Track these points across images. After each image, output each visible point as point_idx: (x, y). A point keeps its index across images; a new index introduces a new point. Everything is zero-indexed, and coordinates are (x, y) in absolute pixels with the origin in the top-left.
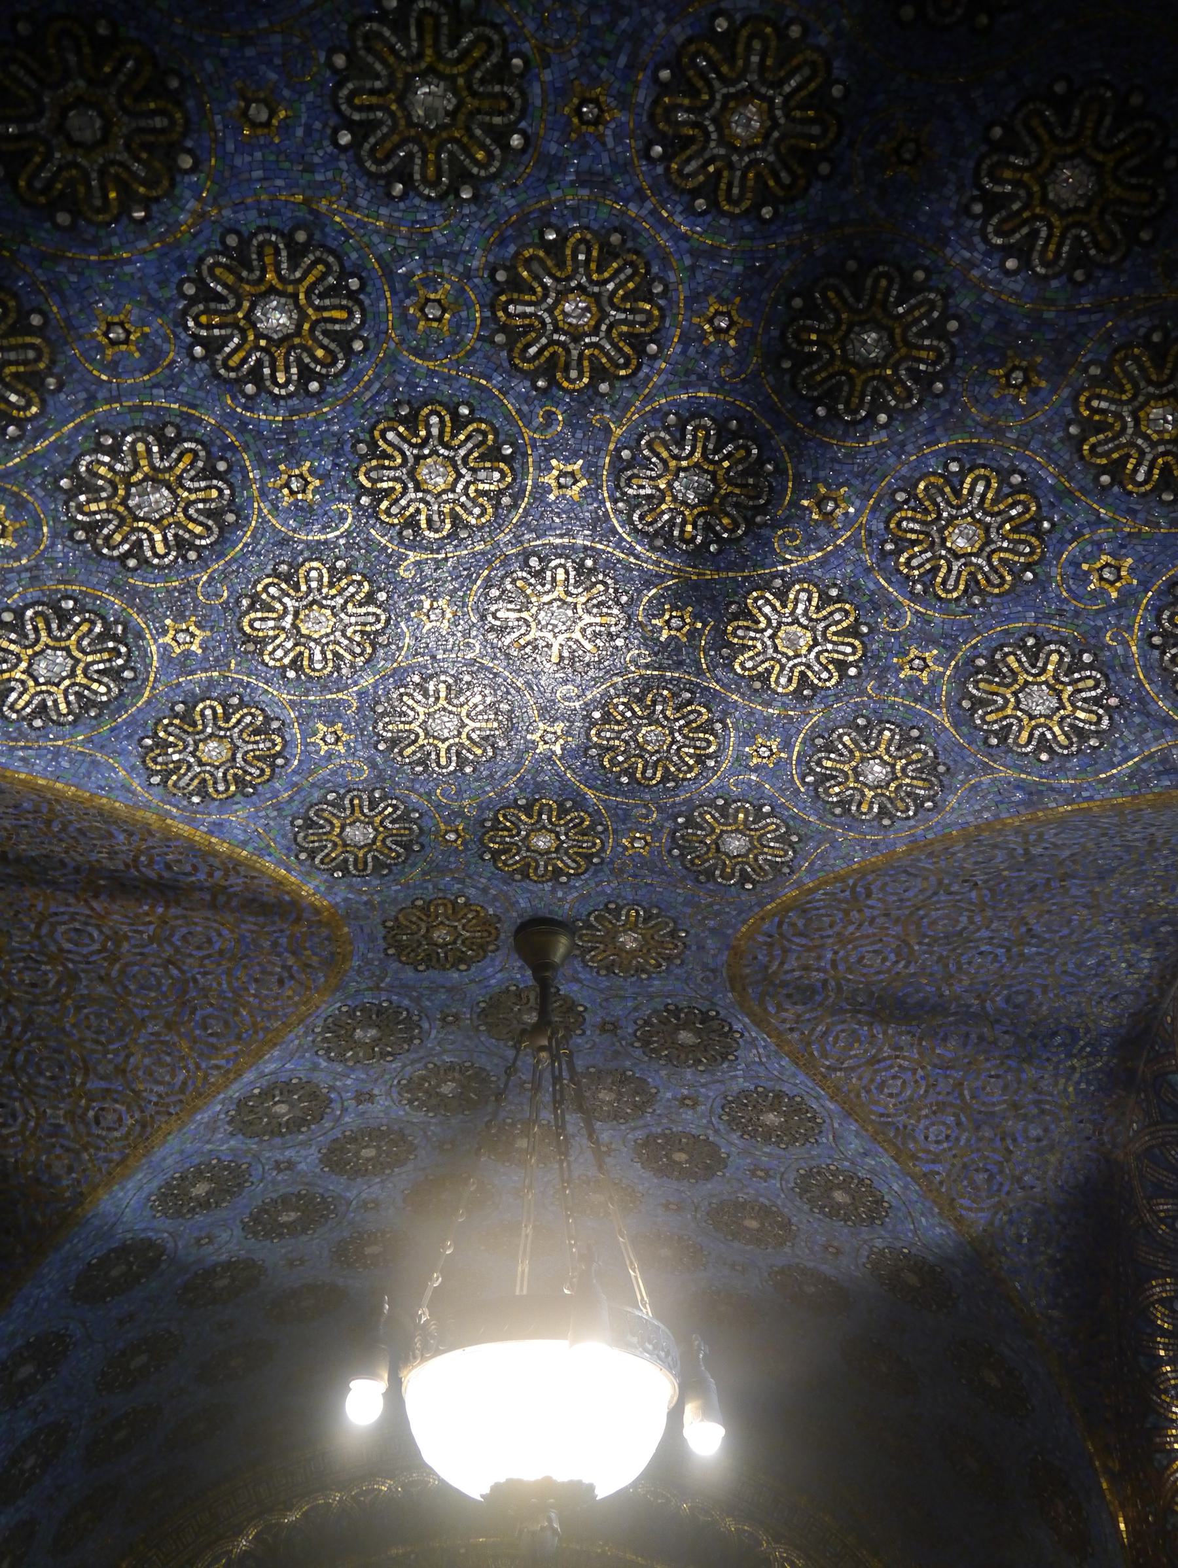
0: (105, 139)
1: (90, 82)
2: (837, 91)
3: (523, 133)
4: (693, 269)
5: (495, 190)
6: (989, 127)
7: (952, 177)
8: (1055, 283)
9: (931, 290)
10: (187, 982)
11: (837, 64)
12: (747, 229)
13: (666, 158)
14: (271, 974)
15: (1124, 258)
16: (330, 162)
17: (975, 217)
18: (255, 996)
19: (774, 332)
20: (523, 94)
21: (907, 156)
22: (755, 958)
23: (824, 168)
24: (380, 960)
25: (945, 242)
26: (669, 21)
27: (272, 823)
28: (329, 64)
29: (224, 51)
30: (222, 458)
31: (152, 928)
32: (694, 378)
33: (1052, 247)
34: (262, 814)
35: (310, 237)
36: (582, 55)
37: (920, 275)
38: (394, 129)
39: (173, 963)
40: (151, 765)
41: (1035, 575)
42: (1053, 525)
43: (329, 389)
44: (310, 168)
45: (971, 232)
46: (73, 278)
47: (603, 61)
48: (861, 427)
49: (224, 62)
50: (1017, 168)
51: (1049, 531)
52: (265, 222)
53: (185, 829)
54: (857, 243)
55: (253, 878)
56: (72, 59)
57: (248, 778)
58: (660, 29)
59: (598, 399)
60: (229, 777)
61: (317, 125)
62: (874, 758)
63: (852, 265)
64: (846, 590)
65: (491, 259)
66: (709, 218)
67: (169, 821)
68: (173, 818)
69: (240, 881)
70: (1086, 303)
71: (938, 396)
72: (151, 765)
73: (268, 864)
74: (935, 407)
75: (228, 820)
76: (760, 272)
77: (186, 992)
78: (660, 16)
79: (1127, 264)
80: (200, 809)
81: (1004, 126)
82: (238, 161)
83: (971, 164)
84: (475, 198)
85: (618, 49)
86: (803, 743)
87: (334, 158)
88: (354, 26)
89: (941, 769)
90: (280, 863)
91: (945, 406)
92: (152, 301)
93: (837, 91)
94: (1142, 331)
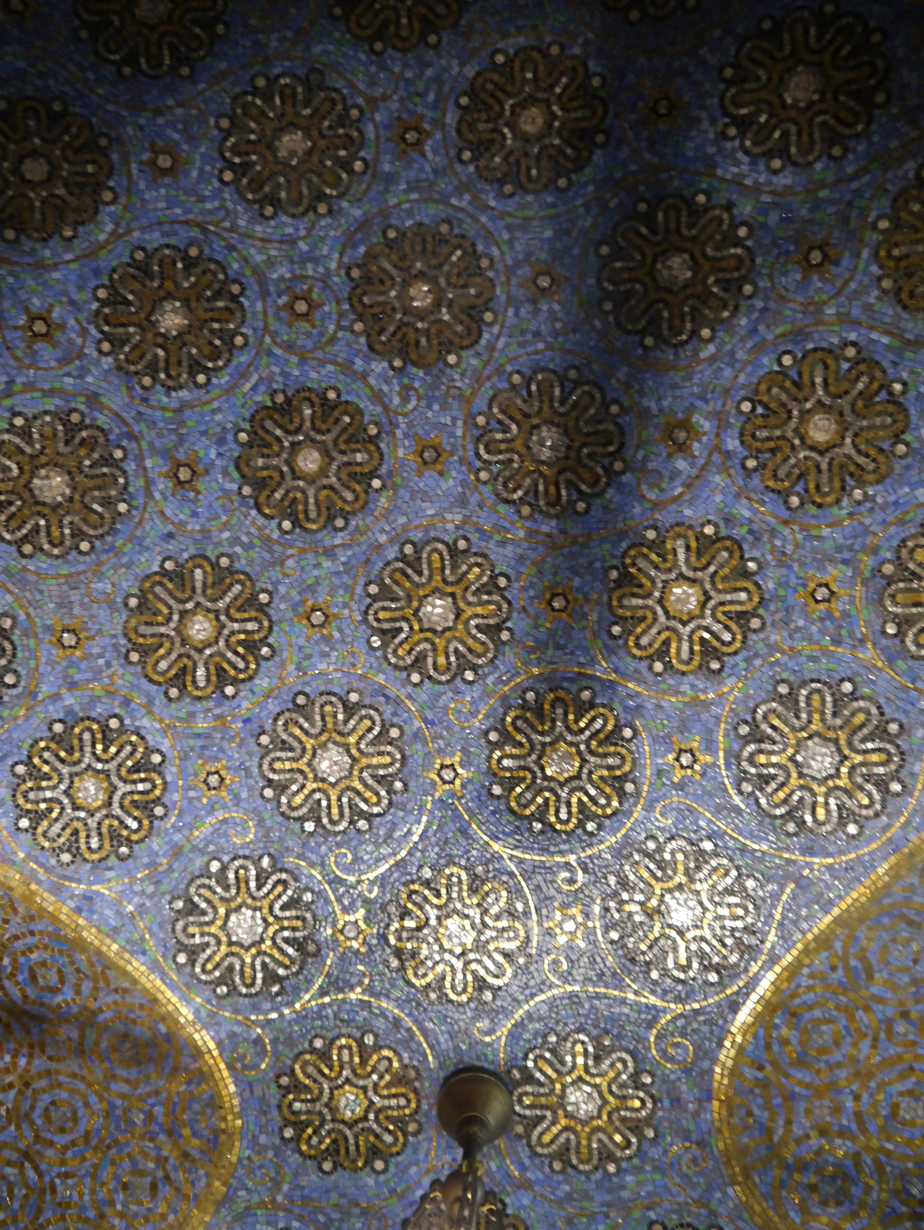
0: (49, 180)
1: (43, 140)
2: (596, 82)
3: (363, 159)
4: (511, 242)
5: (345, 204)
6: (721, 70)
7: (703, 115)
8: (818, 166)
9: (715, 207)
10: (43, 1191)
11: (591, 64)
12: (550, 199)
13: (474, 159)
14: (142, 1174)
15: (868, 124)
16: (217, 194)
17: (732, 139)
18: (122, 1215)
19: (591, 281)
20: (360, 132)
21: (663, 111)
22: (750, 1113)
23: (600, 138)
24: (275, 1148)
25: (713, 166)
26: (462, 64)
27: (148, 904)
28: (217, 126)
29: (142, 121)
30: (119, 447)
31: (12, 1094)
32: (529, 337)
33: (805, 138)
34: (137, 888)
35: (201, 251)
36: (401, 100)
37: (701, 198)
38: (418, 585)
39: (32, 1161)
40: (21, 801)
41: (907, 445)
42: (905, 384)
43: (214, 381)
44: (202, 199)
45: (733, 151)
46: (11, 280)
47: (417, 100)
48: (688, 347)
49: (141, 128)
50: (752, 91)
51: (903, 393)
52: (166, 241)
53: (49, 901)
54: (642, 188)
55: (125, 991)
56: (32, 123)
57: (125, 833)
58: (456, 70)
59: (448, 371)
60: (104, 830)
61: (208, 168)
62: (810, 737)
63: (643, 207)
64: (722, 524)
65: (346, 259)
66: (517, 198)
67: (33, 887)
68: (39, 883)
69: (110, 999)
70: (850, 170)
71: (749, 298)
72: (21, 801)
73: (137, 967)
74: (751, 308)
75: (97, 893)
76: (568, 232)
77: (40, 1211)
78: (454, 63)
79: (874, 127)
80: (69, 871)
81: (732, 66)
82: (147, 196)
83: (716, 101)
84: (330, 212)
85: (427, 90)
86: (726, 735)
87: (221, 191)
88: (235, 99)
89: (893, 728)
90: (155, 967)
91: (759, 304)
92: (72, 302)
93: (596, 82)
94: (911, 175)
